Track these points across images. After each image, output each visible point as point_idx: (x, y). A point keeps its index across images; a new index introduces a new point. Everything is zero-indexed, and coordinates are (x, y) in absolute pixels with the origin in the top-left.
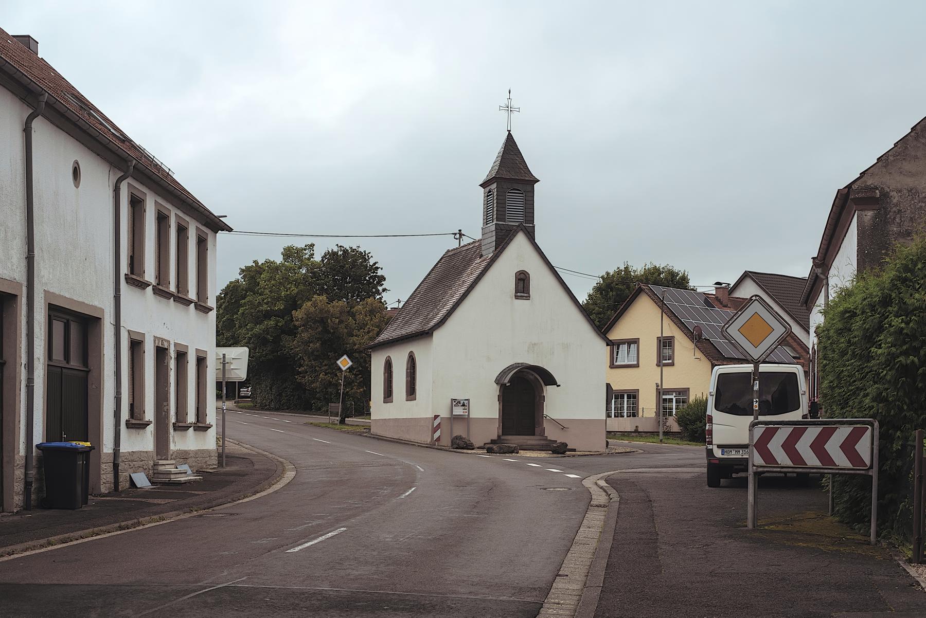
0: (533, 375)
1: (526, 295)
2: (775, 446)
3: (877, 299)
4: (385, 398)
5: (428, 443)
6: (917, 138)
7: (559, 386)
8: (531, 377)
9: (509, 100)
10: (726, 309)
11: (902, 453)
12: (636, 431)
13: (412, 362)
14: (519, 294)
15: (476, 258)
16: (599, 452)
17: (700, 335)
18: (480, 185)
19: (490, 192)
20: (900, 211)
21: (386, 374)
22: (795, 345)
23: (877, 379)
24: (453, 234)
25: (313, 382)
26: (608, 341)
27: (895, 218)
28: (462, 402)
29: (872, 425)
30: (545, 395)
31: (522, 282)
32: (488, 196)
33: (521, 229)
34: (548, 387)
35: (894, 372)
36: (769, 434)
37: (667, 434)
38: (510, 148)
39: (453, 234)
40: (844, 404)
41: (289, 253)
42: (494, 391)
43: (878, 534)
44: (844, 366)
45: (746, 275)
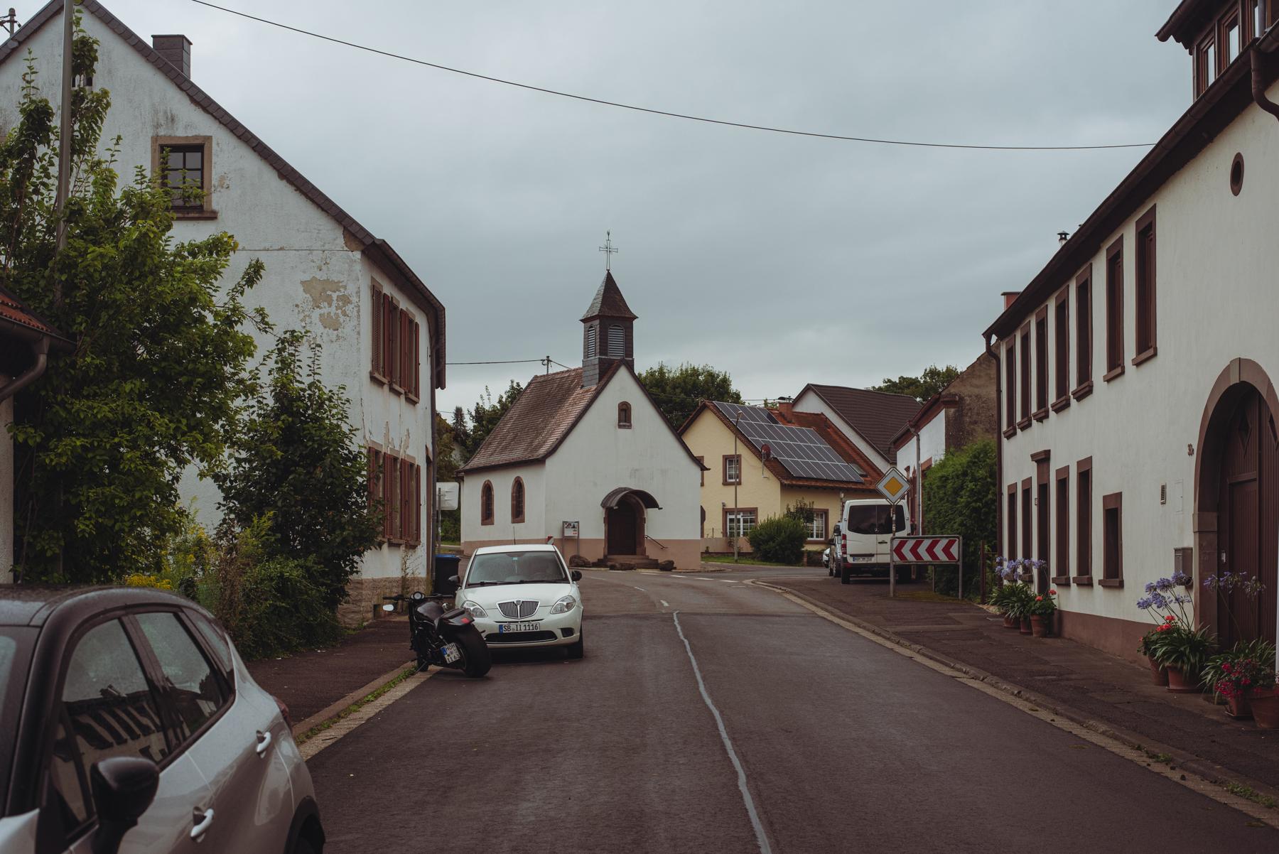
0: (634, 498)
2: (906, 550)
3: (960, 472)
4: (483, 520)
6: (980, 364)
7: (661, 508)
8: (634, 501)
10: (790, 426)
11: (975, 553)
13: (519, 488)
14: (621, 424)
15: (575, 388)
17: (768, 454)
20: (970, 409)
21: (484, 498)
22: (861, 462)
23: (961, 514)
27: (967, 413)
28: (572, 524)
29: (959, 538)
34: (648, 509)
35: (969, 511)
36: (902, 544)
37: (741, 555)
38: (610, 287)
40: (942, 527)
42: (600, 513)
43: (962, 597)
44: (942, 506)
45: (809, 388)
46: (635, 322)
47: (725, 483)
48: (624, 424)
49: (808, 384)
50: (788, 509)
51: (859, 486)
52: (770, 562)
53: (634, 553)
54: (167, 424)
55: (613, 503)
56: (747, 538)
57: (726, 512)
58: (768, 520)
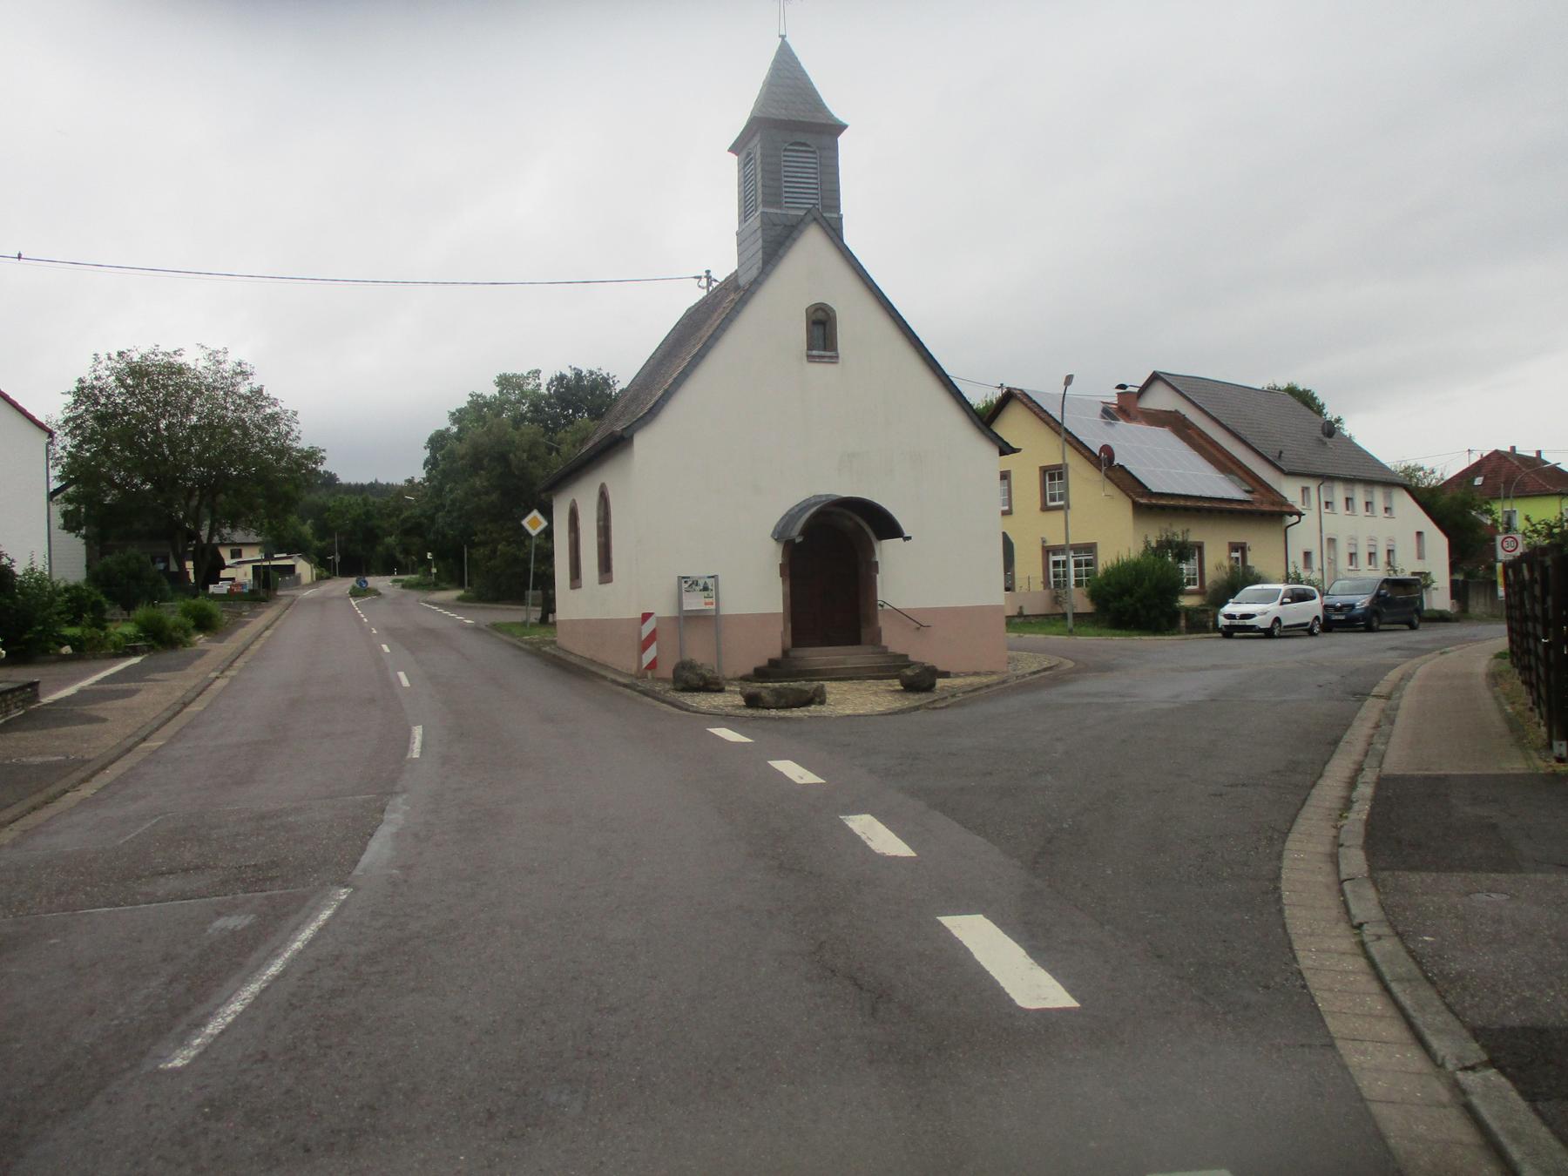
0: (851, 519)
5: (633, 673)
7: (909, 538)
12: (1020, 615)
14: (815, 353)
16: (993, 673)
19: (749, 154)
24: (695, 277)
26: (1001, 443)
28: (701, 583)
30: (877, 560)
31: (821, 327)
32: (745, 165)
33: (815, 219)
39: (695, 277)
41: (505, 382)
42: (770, 556)
45: (1155, 377)
46: (842, 140)
47: (1045, 508)
48: (822, 353)
49: (1154, 372)
50: (1147, 543)
51: (1246, 507)
52: (1126, 629)
53: (855, 640)
54: (456, 483)
55: (795, 533)
56: (1084, 590)
57: (1048, 551)
58: (1118, 561)
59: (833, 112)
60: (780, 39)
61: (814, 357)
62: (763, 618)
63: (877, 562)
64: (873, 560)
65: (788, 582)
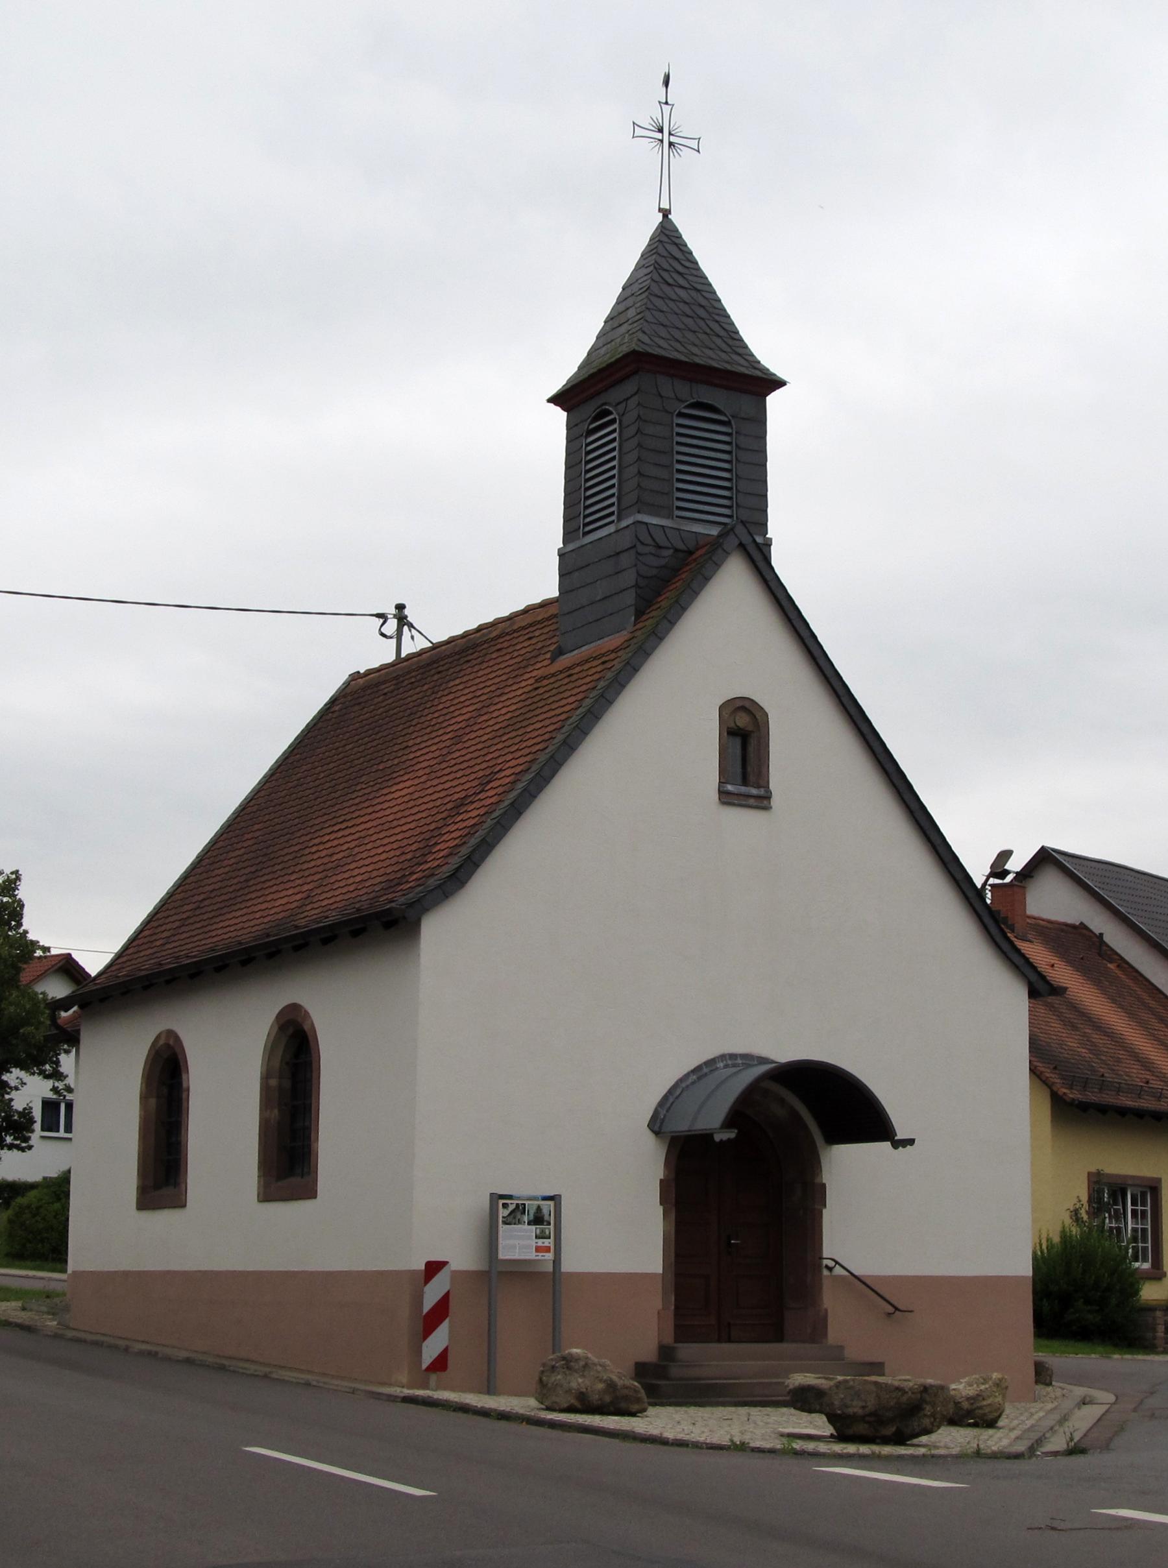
0: (782, 1101)
1: (754, 791)
9: (666, 108)
18: (550, 400)
25: (993, 1446)
30: (824, 1181)
45: (1045, 858)
46: (774, 401)
49: (1043, 847)
59: (759, 357)
60: (661, 214)
61: (729, 793)
62: (656, 1274)
63: (824, 1186)
64: (817, 1181)
65: (673, 1216)
